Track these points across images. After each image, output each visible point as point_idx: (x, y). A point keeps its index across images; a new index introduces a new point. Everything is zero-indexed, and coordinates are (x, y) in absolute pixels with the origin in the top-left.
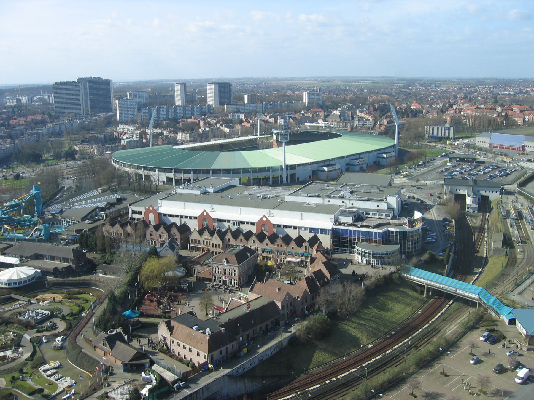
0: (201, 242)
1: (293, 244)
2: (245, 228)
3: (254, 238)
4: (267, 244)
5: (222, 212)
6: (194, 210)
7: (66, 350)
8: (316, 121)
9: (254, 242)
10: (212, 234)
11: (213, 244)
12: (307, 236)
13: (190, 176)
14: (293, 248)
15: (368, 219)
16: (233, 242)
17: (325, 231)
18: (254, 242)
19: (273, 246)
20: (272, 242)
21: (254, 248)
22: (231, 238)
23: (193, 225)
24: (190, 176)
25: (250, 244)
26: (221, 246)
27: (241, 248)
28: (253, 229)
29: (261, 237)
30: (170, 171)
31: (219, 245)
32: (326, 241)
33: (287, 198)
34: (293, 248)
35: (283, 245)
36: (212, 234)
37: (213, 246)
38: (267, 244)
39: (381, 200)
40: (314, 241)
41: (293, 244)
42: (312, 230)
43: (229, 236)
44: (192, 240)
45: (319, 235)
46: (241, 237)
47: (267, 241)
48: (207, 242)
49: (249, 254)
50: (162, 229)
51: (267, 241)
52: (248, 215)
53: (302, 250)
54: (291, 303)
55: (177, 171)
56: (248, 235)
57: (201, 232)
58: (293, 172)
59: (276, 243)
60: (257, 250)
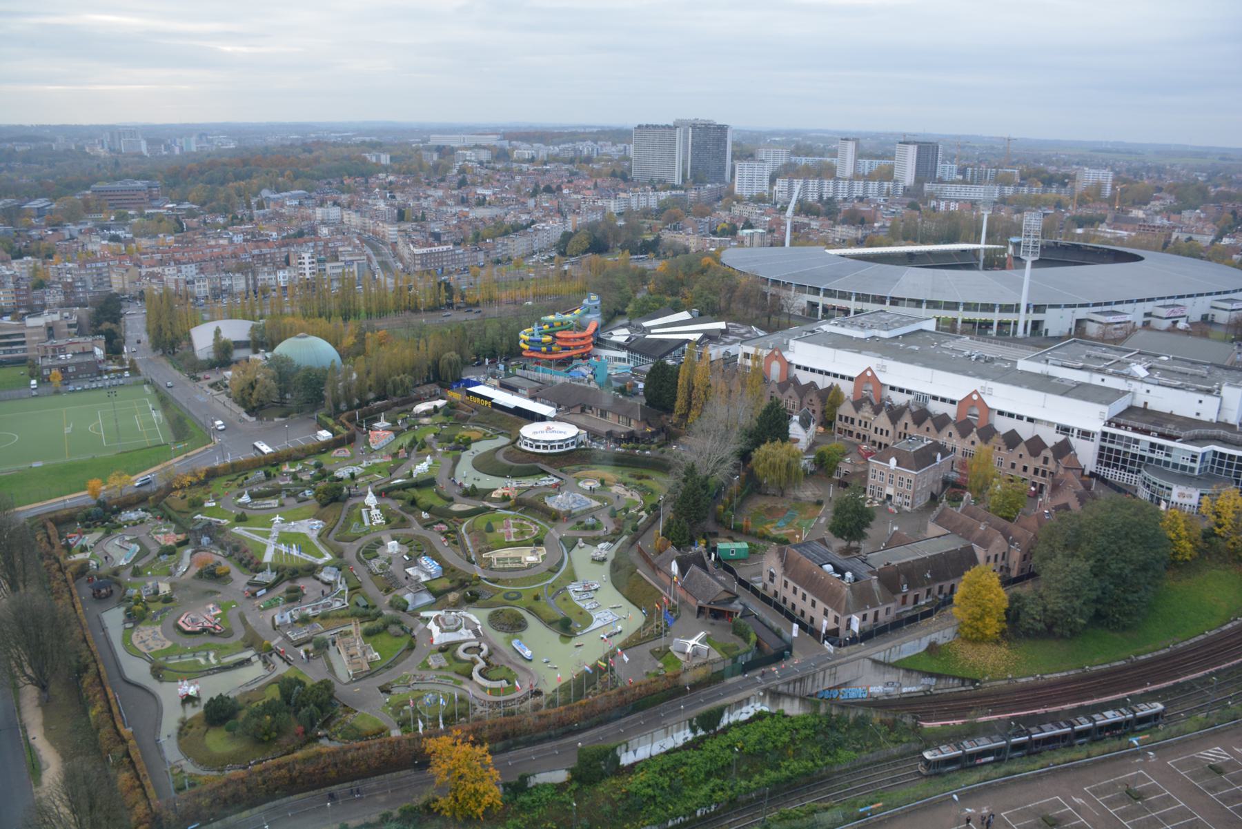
0: (856, 422)
1: (1022, 449)
2: (936, 408)
3: (951, 428)
5: (906, 378)
6: (851, 364)
9: (950, 435)
10: (877, 411)
12: (1051, 438)
13: (852, 305)
16: (912, 429)
17: (1086, 434)
18: (950, 435)
19: (985, 447)
20: (964, 435)
21: (949, 446)
22: (910, 424)
23: (847, 388)
24: (852, 305)
25: (943, 439)
28: (952, 411)
29: (964, 428)
30: (816, 291)
32: (1087, 454)
33: (1023, 365)
35: (1004, 447)
36: (877, 411)
38: (973, 443)
39: (1209, 392)
40: (1063, 449)
41: (1022, 449)
42: (1065, 430)
44: (841, 417)
45: (1074, 441)
46: (928, 423)
47: (974, 436)
49: (939, 455)
50: (791, 391)
51: (974, 436)
52: (945, 387)
53: (1038, 463)
55: (829, 293)
56: (941, 422)
57: (857, 405)
58: (1038, 317)
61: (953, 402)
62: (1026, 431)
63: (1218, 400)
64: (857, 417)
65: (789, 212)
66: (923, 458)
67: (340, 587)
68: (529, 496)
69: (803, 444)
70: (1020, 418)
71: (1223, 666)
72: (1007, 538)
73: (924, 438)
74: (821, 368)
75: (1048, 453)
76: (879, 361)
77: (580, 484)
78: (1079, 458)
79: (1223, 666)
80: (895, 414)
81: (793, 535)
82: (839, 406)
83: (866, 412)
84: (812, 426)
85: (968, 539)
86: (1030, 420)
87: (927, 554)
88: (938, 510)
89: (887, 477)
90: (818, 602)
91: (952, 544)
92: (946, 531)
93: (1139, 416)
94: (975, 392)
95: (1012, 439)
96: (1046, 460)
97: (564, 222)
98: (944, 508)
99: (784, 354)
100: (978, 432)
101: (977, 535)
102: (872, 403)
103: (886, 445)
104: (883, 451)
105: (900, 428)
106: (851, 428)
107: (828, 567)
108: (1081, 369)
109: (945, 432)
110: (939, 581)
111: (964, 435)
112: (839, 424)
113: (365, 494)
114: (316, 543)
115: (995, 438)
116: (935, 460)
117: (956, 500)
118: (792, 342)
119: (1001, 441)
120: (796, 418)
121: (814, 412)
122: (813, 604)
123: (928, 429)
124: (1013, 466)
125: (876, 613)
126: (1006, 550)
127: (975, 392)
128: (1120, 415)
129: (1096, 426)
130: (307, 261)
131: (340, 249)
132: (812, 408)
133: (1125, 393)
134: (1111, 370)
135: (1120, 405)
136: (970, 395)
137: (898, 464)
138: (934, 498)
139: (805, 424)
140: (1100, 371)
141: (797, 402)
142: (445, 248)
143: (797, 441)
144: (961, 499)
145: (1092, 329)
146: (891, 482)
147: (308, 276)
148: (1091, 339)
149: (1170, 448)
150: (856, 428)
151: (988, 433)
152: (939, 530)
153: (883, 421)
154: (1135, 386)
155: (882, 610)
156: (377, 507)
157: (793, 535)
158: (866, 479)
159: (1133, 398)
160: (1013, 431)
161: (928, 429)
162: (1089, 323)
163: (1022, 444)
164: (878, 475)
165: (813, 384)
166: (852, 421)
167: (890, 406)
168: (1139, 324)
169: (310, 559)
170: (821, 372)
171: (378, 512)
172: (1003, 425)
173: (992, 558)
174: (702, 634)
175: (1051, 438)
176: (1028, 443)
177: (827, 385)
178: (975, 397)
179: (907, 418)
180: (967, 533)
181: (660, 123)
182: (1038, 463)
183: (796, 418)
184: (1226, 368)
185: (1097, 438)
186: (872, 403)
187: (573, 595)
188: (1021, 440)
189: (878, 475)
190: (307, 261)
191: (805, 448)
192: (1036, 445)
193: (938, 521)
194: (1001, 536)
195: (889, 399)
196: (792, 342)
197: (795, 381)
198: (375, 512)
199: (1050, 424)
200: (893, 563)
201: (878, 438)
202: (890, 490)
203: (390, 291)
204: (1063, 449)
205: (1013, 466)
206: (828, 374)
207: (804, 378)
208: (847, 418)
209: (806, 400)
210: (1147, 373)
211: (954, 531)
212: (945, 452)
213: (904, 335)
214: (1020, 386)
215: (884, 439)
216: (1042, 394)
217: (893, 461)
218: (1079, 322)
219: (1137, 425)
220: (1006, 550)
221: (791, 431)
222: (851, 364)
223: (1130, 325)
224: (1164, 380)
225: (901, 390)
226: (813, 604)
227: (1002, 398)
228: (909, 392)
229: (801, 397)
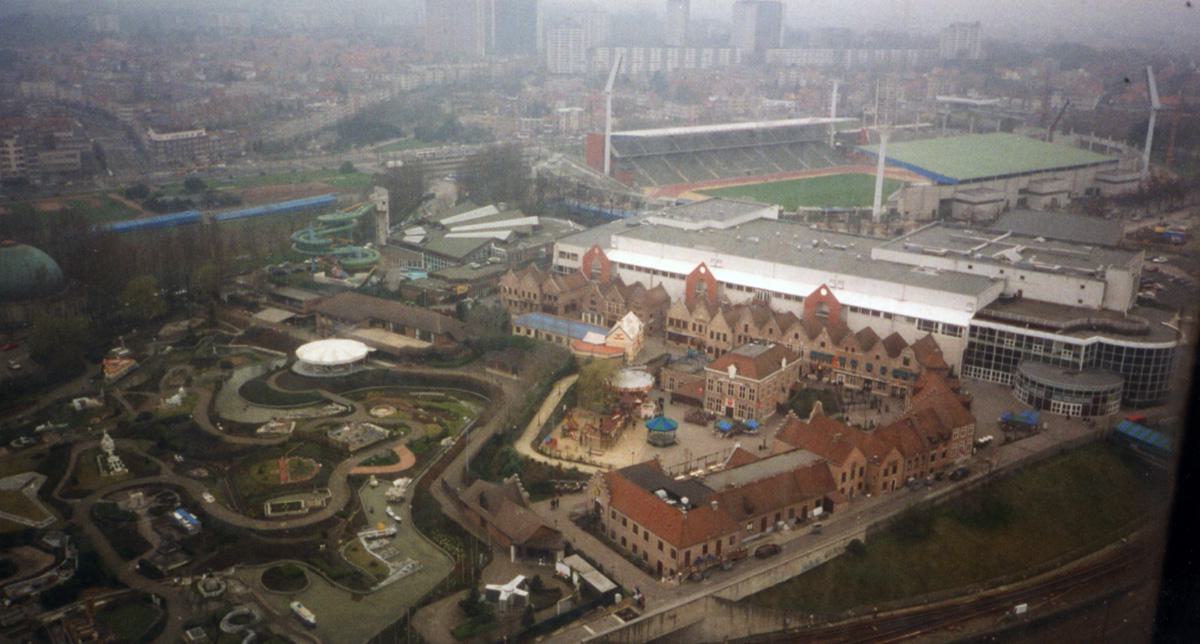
0: (690, 327)
1: (880, 351)
3: (797, 329)
4: (823, 345)
9: (797, 336)
18: (797, 336)
23: (676, 289)
25: (788, 341)
28: (798, 309)
37: (712, 336)
39: (1091, 276)
42: (928, 325)
44: (671, 321)
45: (940, 337)
48: (700, 327)
49: (784, 361)
56: (787, 321)
61: (798, 299)
62: (882, 329)
63: (1102, 284)
65: (609, 87)
66: (763, 366)
67: (68, 554)
68: (309, 428)
70: (876, 313)
74: (649, 266)
75: (907, 353)
76: (713, 255)
77: (373, 412)
78: (945, 357)
80: (733, 313)
83: (701, 314)
86: (888, 316)
89: (725, 389)
90: (651, 535)
93: (1007, 303)
94: (824, 286)
95: (868, 339)
96: (906, 362)
97: (343, 103)
99: (605, 251)
103: (724, 352)
104: (720, 357)
107: (661, 493)
108: (944, 255)
109: (791, 333)
113: (101, 436)
114: (37, 502)
118: (614, 238)
122: (646, 537)
125: (719, 544)
127: (824, 286)
128: (992, 306)
129: (963, 318)
130: (12, 149)
131: (57, 134)
133: (994, 281)
134: (979, 255)
135: (991, 294)
136: (818, 291)
137: (738, 372)
140: (967, 257)
142: (195, 133)
145: (959, 210)
147: (14, 169)
148: (957, 220)
149: (1049, 343)
150: (690, 333)
151: (840, 333)
153: (719, 324)
154: (1009, 272)
155: (725, 541)
156: (115, 453)
159: (1006, 286)
162: (955, 204)
165: (638, 284)
166: (685, 325)
168: (1013, 203)
169: (28, 522)
170: (647, 270)
171: (117, 459)
172: (857, 323)
174: (520, 578)
175: (911, 335)
176: (859, 335)
177: (655, 284)
178: (824, 292)
182: (897, 364)
184: (1111, 248)
185: (966, 333)
187: (365, 544)
188: (878, 338)
190: (12, 149)
192: (895, 344)
195: (726, 298)
196: (614, 238)
197: (619, 281)
198: (113, 459)
199: (911, 320)
204: (927, 347)
206: (655, 272)
207: (629, 277)
208: (678, 322)
210: (384, 243)
212: (791, 356)
213: (742, 225)
214: (752, 257)
215: (722, 345)
216: (900, 286)
217: (732, 369)
218: (943, 202)
219: (1036, 320)
222: (680, 261)
223: (1002, 205)
224: (1040, 264)
225: (740, 288)
226: (646, 537)
227: (853, 293)
228: (749, 289)
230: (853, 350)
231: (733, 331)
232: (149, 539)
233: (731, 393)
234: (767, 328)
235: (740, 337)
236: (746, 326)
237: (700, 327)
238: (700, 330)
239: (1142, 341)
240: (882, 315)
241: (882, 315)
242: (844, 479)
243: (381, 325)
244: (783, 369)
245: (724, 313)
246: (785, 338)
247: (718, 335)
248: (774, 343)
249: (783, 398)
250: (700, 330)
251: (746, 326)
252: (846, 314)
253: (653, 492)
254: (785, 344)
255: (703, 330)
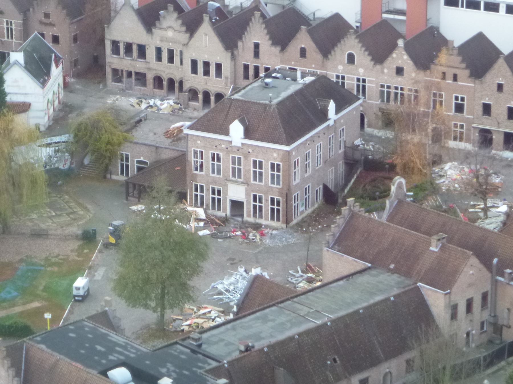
0: (151, 53)
3: (351, 45)
4: (399, 71)
7: (166, 95)
8: (140, 158)
9: (351, 59)
10: (191, 26)
11: (194, 63)
14: (500, 87)
15: (123, 60)
16: (271, 57)
18: (351, 59)
19: (423, 76)
20: (379, 56)
21: (351, 83)
22: (266, 45)
25: (336, 69)
26: (226, 70)
27: (302, 81)
31: (219, 67)
34: (500, 87)
35: (464, 74)
36: (191, 26)
37: (194, 70)
38: (399, 71)
43: (257, 34)
44: (115, 44)
46: (303, 40)
47: (400, 57)
48: (171, 53)
49: (332, 106)
51: (400, 57)
54: (485, 297)
56: (331, 33)
59: (437, 69)
60: (362, 89)
64: (151, 42)
66: (299, 116)
69: (39, 115)
71: (23, 368)
72: (486, 263)
73: (297, 70)
79: (23, 368)
81: (39, 312)
82: (109, 20)
84: (56, 72)
85: (407, 274)
87: (327, 317)
88: (340, 220)
89: (226, 165)
91: (383, 286)
92: (361, 264)
98: (353, 215)
100: (408, 48)
101: (425, 263)
102: (179, 9)
103: (219, 96)
105: (246, 56)
106: (139, 66)
109: (340, 54)
110: (360, 369)
111: (379, 56)
112: (113, 61)
115: (443, 57)
116: (324, 117)
117: (374, 195)
119: (457, 60)
120: (17, 57)
121: (56, 39)
123: (303, 53)
124: (487, 109)
126: (488, 288)
132: (49, 32)
137: (248, 134)
138: (331, 198)
139: (39, 69)
141: (17, 23)
143: (24, 108)
144: (386, 193)
146: (237, 173)
150: (151, 66)
152: (348, 264)
153: (207, 44)
157: (39, 312)
158: (183, 172)
160: (480, 38)
161: (303, 53)
163: (501, 63)
164: (208, 162)
166: (142, 50)
167: (219, 11)
173: (462, 308)
179: (257, 34)
180: (405, 262)
181: (428, 10)
183: (17, 57)
186: (179, 9)
188: (502, 53)
189: (208, 162)
191: (44, 121)
193: (343, 244)
194: (474, 261)
200: (258, 345)
201: (199, 82)
202: (236, 192)
203: (399, 280)
205: (487, 109)
208: (129, 47)
209: (37, 15)
211: (377, 261)
215: (213, 84)
217: (236, 129)
220: (488, 288)
221: (8, 88)
229: (25, 12)
230: (455, 78)
231: (233, 57)
232: (250, 77)
233: (237, 173)
234: (294, 47)
235: (246, 67)
236: (257, 46)
237: (171, 53)
238: (171, 60)
239: (350, 106)
240: (503, 9)
241: (503, 9)
242: (454, 316)
243: (489, 178)
244: (331, 123)
245: (139, 101)
246: (329, 64)
247: (206, 64)
248: (313, 74)
249: (331, 177)
250: (171, 60)
251: (257, 46)
252: (439, 12)
253: (104, 373)
254: (332, 76)
255: (177, 59)
